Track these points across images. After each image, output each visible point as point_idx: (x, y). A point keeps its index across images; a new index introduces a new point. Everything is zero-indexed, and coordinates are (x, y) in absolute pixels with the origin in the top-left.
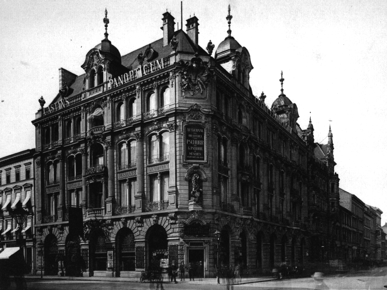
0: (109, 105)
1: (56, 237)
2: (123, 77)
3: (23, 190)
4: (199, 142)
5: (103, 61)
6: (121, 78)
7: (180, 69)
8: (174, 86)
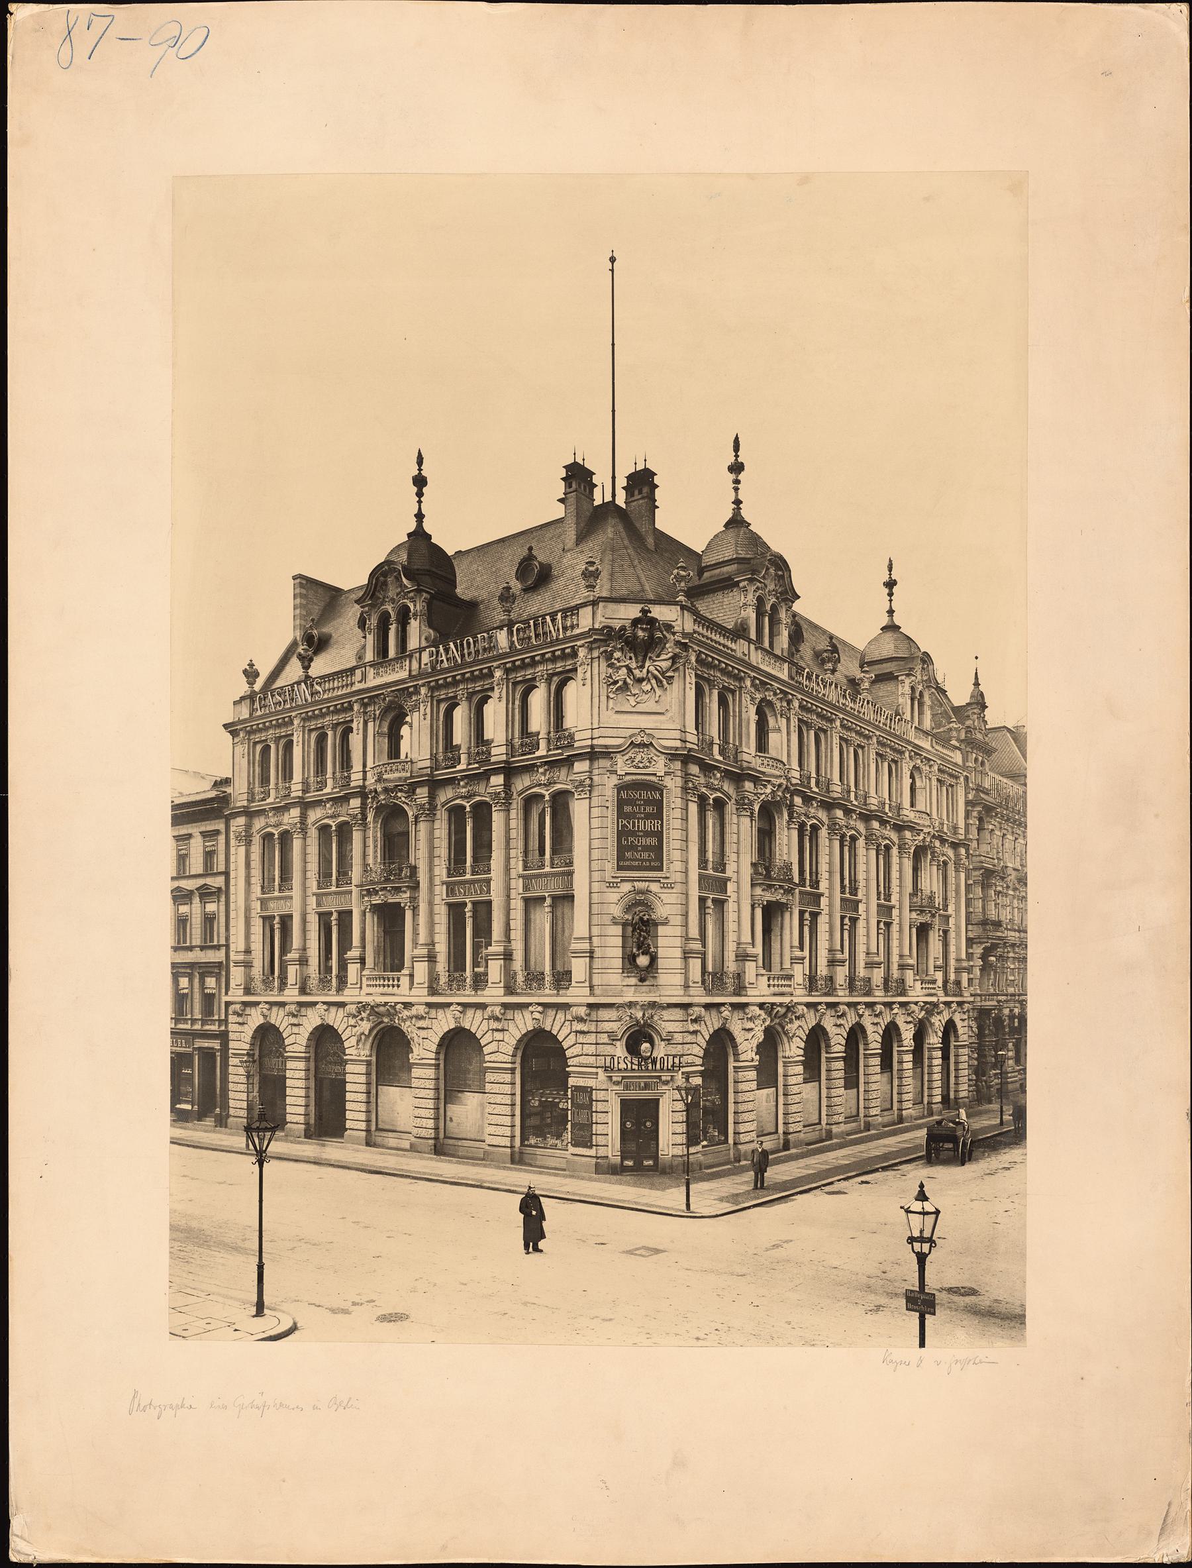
0: (425, 708)
1: (281, 1034)
2: (462, 645)
3: (196, 900)
4: (649, 825)
5: (412, 594)
6: (456, 647)
7: (605, 642)
8: (588, 682)
